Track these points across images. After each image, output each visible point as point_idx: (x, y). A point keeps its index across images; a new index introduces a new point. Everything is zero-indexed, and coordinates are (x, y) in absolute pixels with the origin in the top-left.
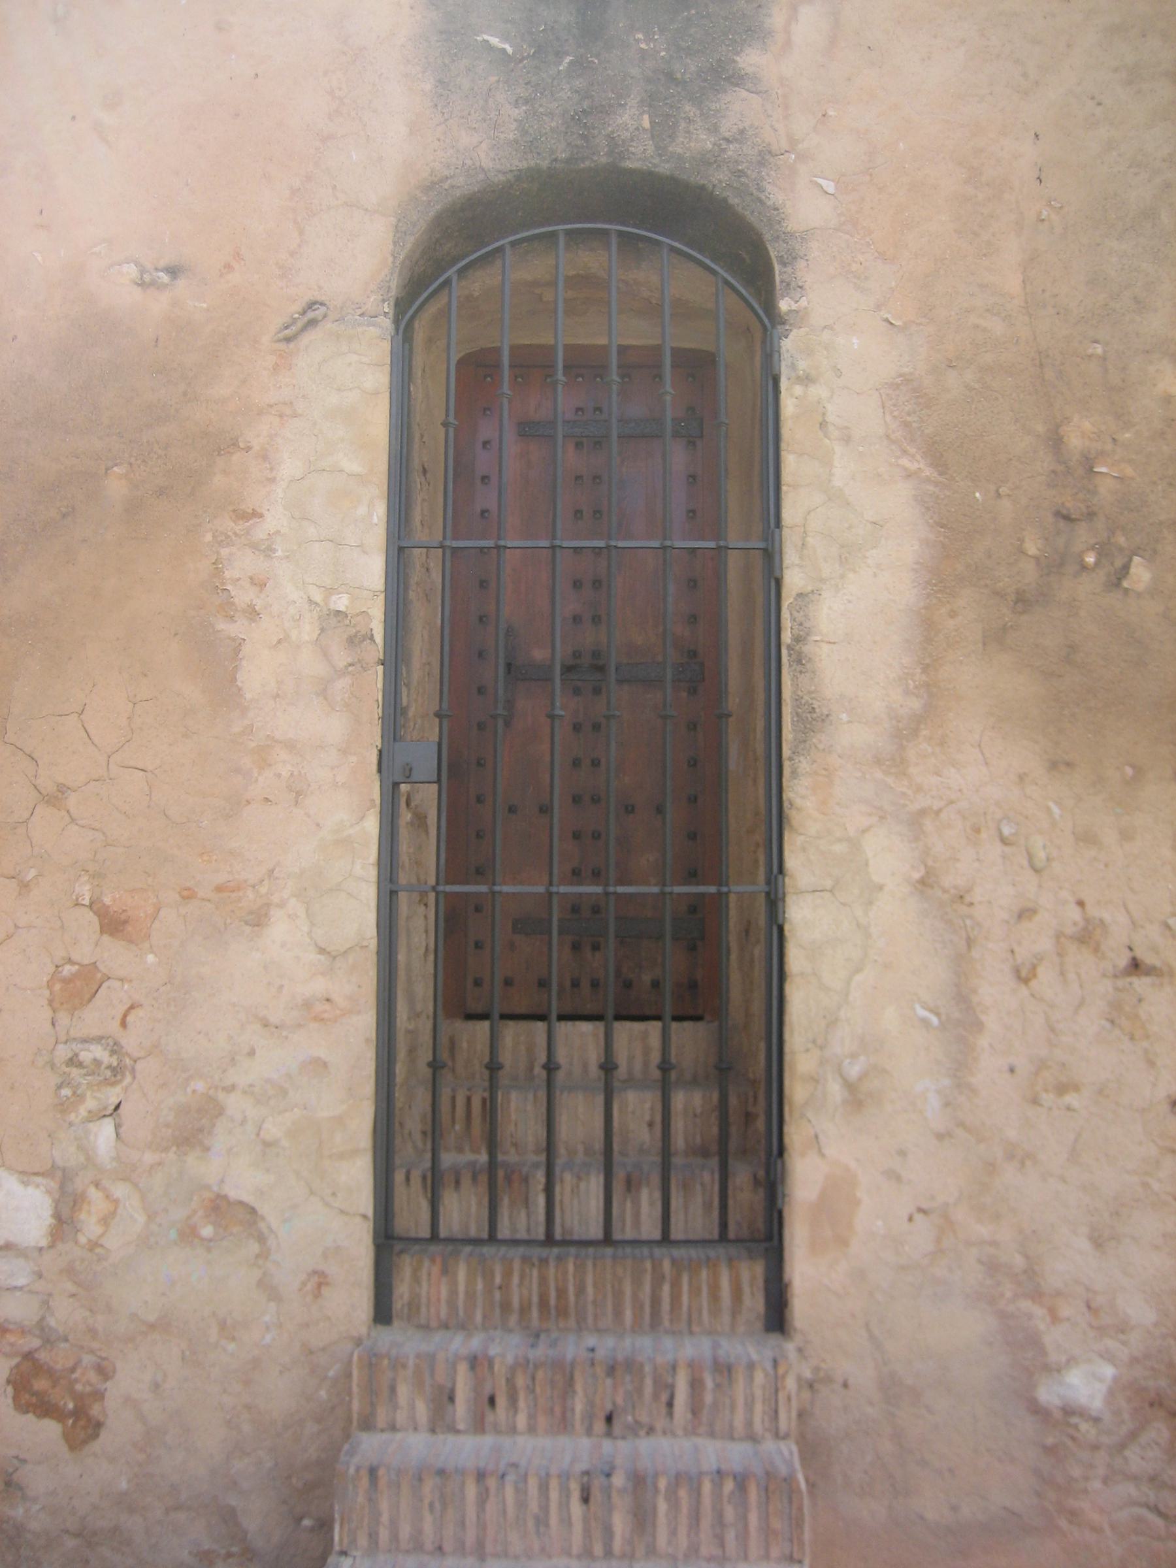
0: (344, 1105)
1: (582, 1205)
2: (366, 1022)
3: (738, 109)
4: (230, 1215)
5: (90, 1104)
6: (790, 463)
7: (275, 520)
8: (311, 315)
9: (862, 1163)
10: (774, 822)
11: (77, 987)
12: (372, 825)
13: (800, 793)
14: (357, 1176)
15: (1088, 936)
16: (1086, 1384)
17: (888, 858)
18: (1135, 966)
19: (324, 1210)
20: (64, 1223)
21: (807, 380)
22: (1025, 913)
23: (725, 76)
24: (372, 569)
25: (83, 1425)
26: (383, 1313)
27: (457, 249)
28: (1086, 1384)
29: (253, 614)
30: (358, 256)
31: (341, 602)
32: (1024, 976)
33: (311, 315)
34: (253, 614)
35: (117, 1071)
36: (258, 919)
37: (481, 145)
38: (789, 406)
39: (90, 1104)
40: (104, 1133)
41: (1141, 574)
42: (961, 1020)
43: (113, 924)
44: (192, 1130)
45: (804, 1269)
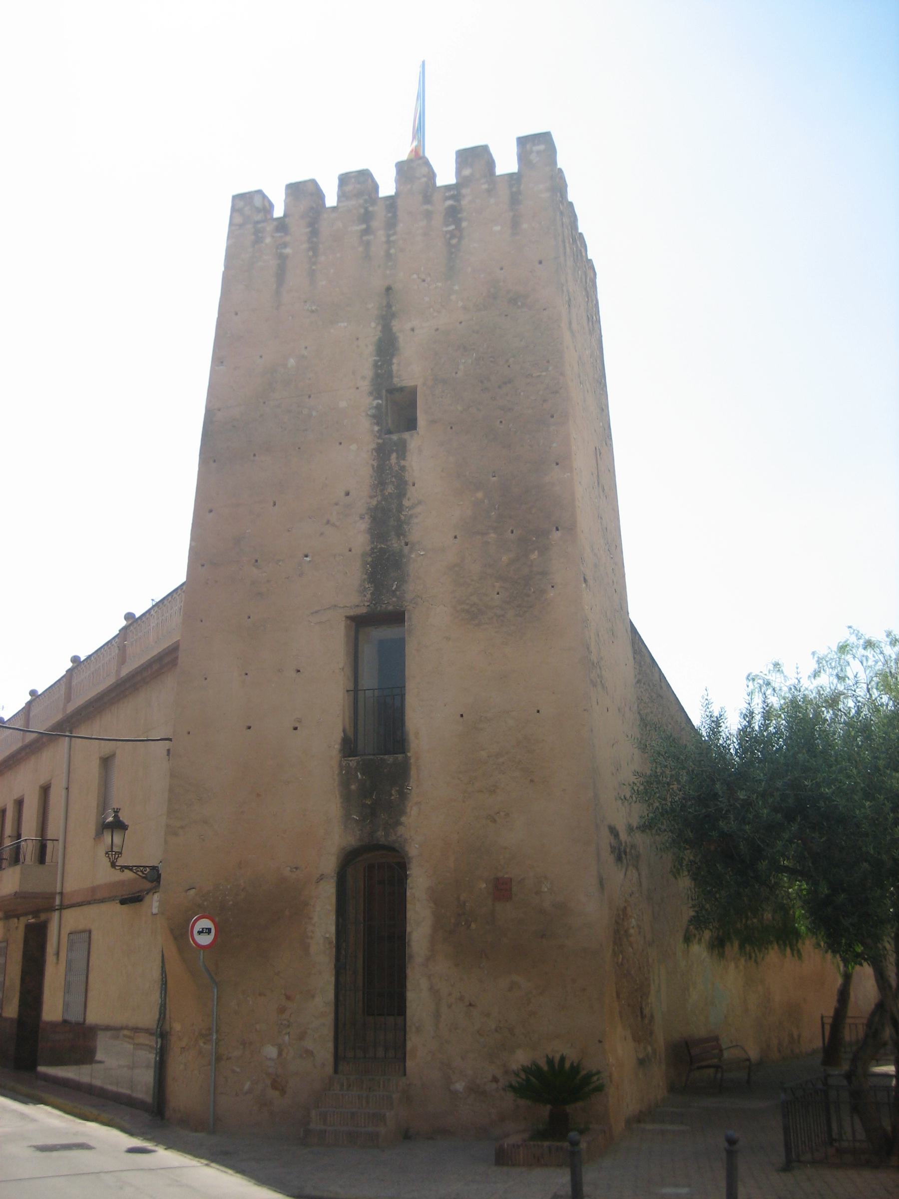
0: (328, 1031)
1: (380, 1053)
2: (332, 1016)
3: (401, 830)
4: (309, 1053)
5: (284, 1032)
6: (408, 906)
7: (316, 919)
8: (322, 877)
9: (421, 1044)
10: (62, 1067)
11: (282, 1010)
12: (333, 979)
13: (409, 972)
14: (330, 1045)
15: (461, 999)
16: (459, 1086)
17: (424, 984)
18: (470, 1005)
19: (324, 1052)
20: (280, 1054)
21: (412, 888)
22: (450, 994)
23: (398, 823)
24: (333, 929)
25: (283, 1092)
26: (336, 1071)
27: (349, 860)
28: (459, 1086)
29: (312, 938)
30: (329, 864)
31: (328, 936)
32: (450, 1006)
33: (322, 877)
34: (312, 938)
35: (289, 1026)
36: (313, 997)
37: (351, 840)
38: (408, 894)
39: (284, 1032)
40: (287, 1037)
41: (473, 926)
42: (437, 1015)
43: (288, 998)
44: (302, 1037)
45: (409, 1063)
